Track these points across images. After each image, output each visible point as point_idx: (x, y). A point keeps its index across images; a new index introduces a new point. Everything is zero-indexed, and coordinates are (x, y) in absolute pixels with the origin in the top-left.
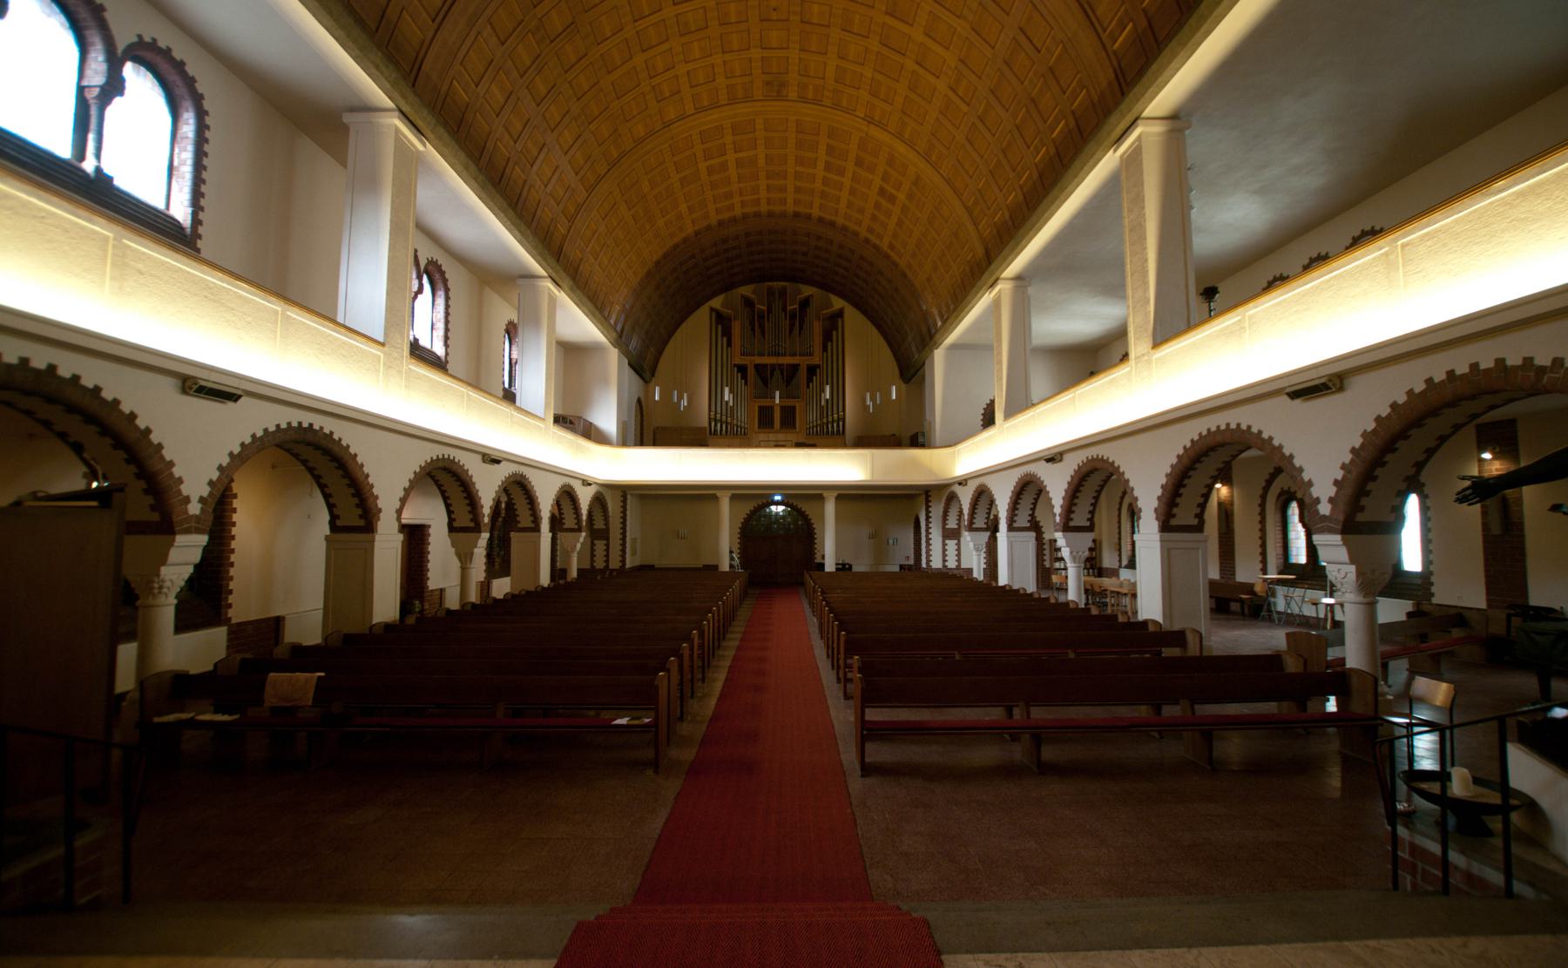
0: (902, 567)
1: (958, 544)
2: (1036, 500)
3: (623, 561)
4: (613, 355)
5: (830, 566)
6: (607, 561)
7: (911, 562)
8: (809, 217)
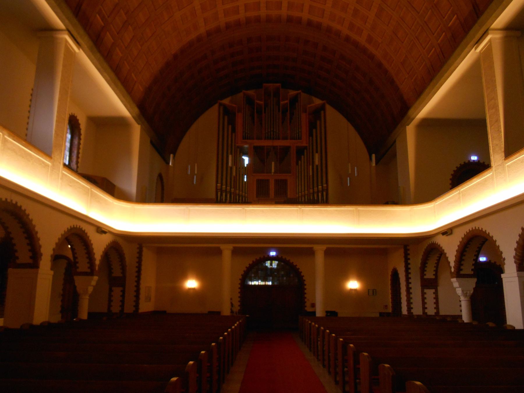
0: (381, 314)
1: (436, 293)
2: (439, 260)
3: (137, 306)
4: (136, 130)
5: (320, 313)
6: (122, 306)
7: (390, 310)
8: (299, 21)
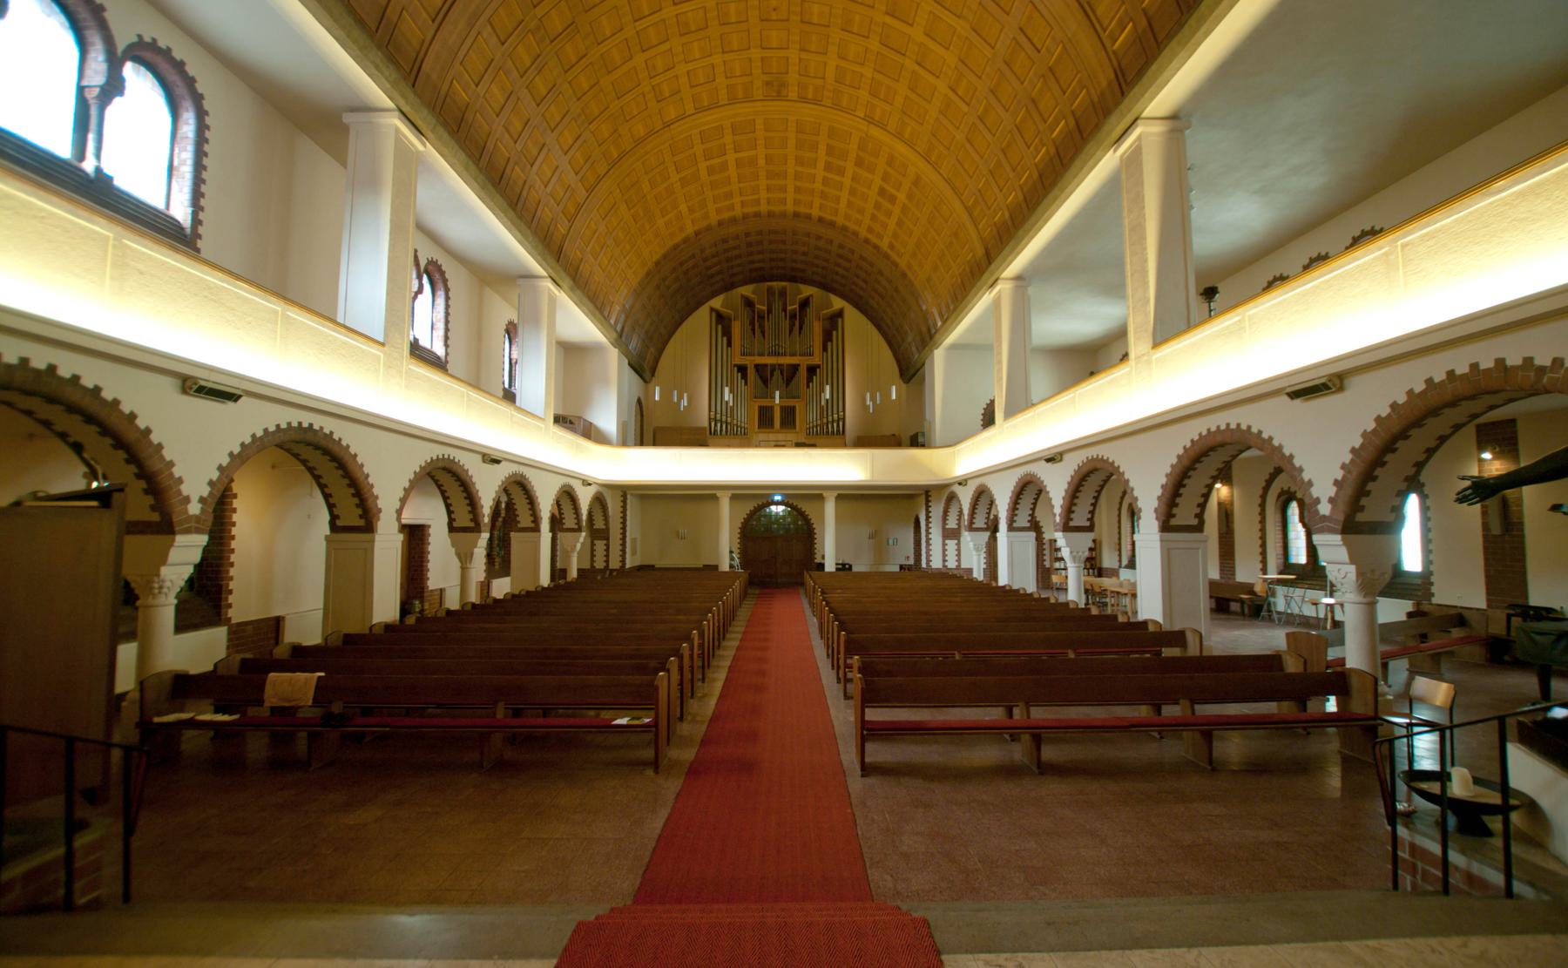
1: (958, 544)
5: (830, 567)
7: (911, 562)
8: (808, 217)
